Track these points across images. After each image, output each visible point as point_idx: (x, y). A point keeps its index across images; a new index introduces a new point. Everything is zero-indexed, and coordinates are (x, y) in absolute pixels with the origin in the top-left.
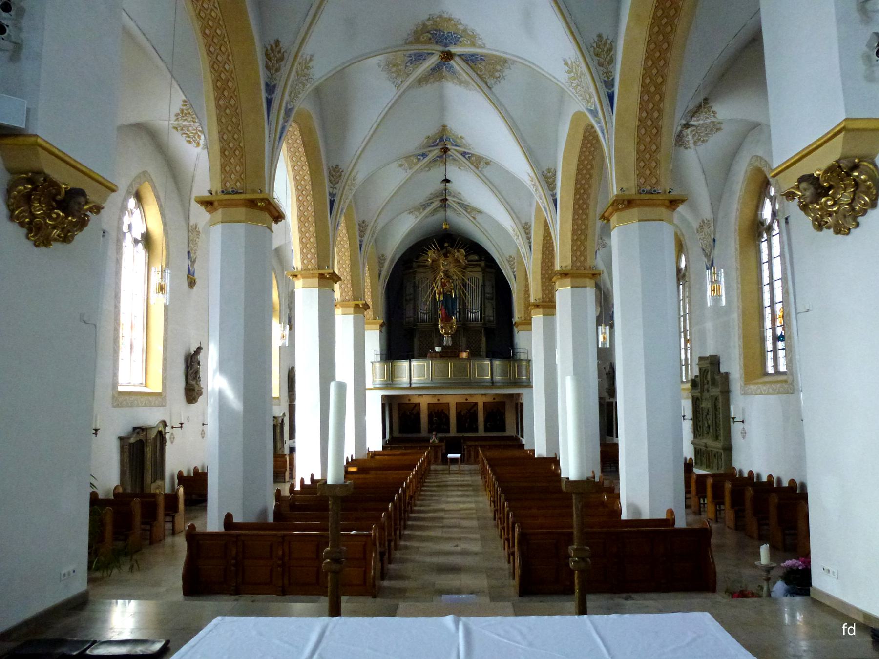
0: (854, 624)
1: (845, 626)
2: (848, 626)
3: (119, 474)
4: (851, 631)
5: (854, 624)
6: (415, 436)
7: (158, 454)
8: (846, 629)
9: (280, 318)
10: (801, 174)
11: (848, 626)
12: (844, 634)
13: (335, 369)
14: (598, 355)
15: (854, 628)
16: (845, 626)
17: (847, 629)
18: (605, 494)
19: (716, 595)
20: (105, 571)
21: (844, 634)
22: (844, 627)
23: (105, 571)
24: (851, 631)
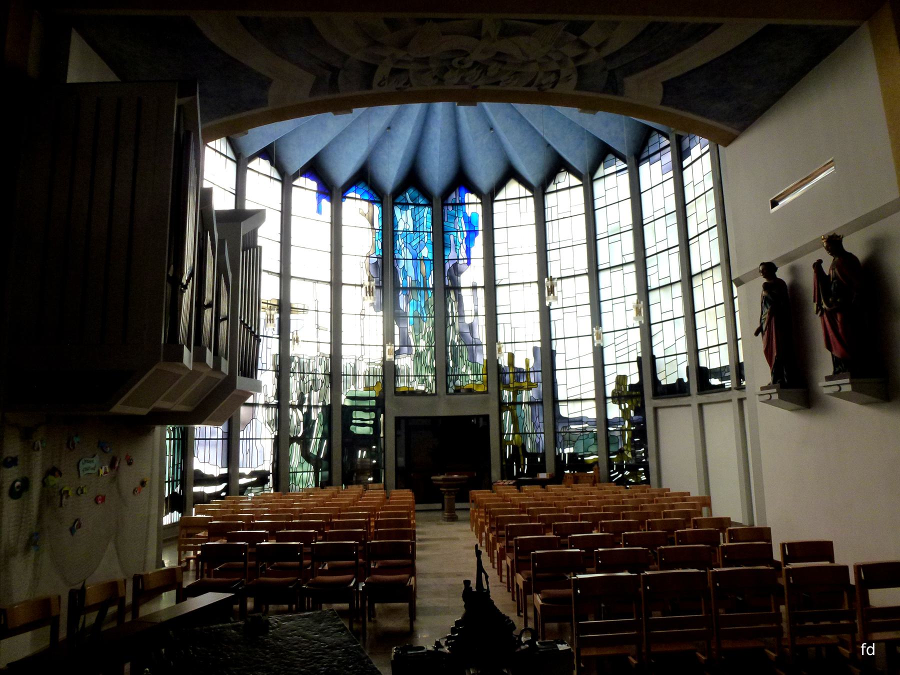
0: (874, 644)
1: (864, 645)
2: (867, 646)
3: (874, 563)
4: (871, 651)
5: (874, 644)
6: (414, 586)
7: (182, 120)
8: (865, 649)
9: (636, 39)
10: (762, 262)
11: (867, 646)
12: (863, 654)
13: (204, 156)
14: (646, 437)
15: (873, 648)
16: (864, 645)
17: (866, 648)
18: (363, 547)
19: (332, 487)
20: (699, 149)
21: (863, 654)
22: (863, 647)
23: (699, 149)
24: (871, 651)
